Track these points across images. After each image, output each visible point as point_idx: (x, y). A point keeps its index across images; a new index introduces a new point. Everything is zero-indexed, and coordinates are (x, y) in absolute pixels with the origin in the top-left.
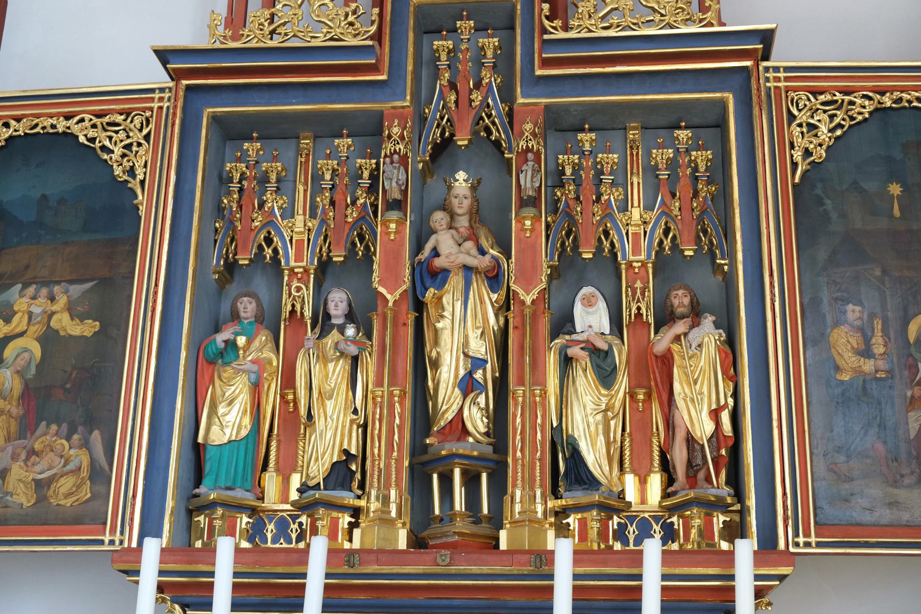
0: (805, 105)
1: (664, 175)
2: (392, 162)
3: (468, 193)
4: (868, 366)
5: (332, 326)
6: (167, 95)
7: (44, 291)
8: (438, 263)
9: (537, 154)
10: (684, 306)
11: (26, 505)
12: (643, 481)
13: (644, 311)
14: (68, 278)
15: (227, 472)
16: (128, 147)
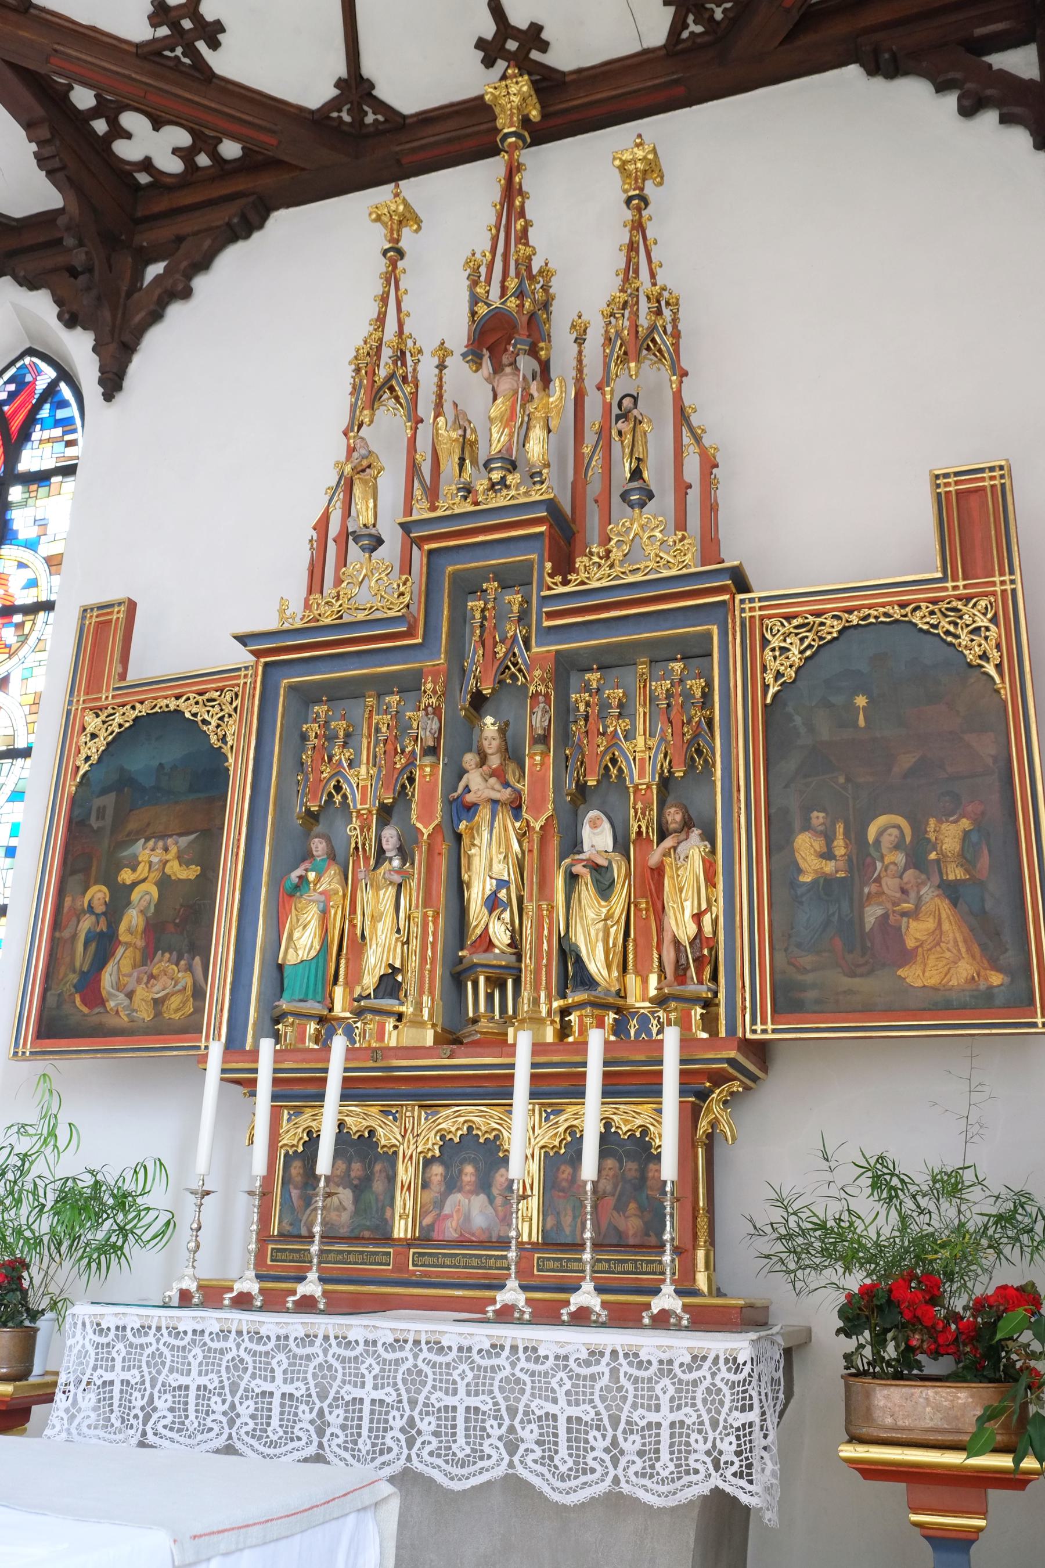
0: (779, 631)
1: (663, 704)
2: (427, 714)
3: (496, 735)
4: (829, 867)
5: (386, 859)
6: (250, 672)
7: (160, 844)
8: (470, 798)
9: (547, 696)
10: (676, 822)
11: (147, 1019)
12: (645, 981)
13: (644, 829)
14: (178, 831)
15: (301, 987)
16: (221, 719)
